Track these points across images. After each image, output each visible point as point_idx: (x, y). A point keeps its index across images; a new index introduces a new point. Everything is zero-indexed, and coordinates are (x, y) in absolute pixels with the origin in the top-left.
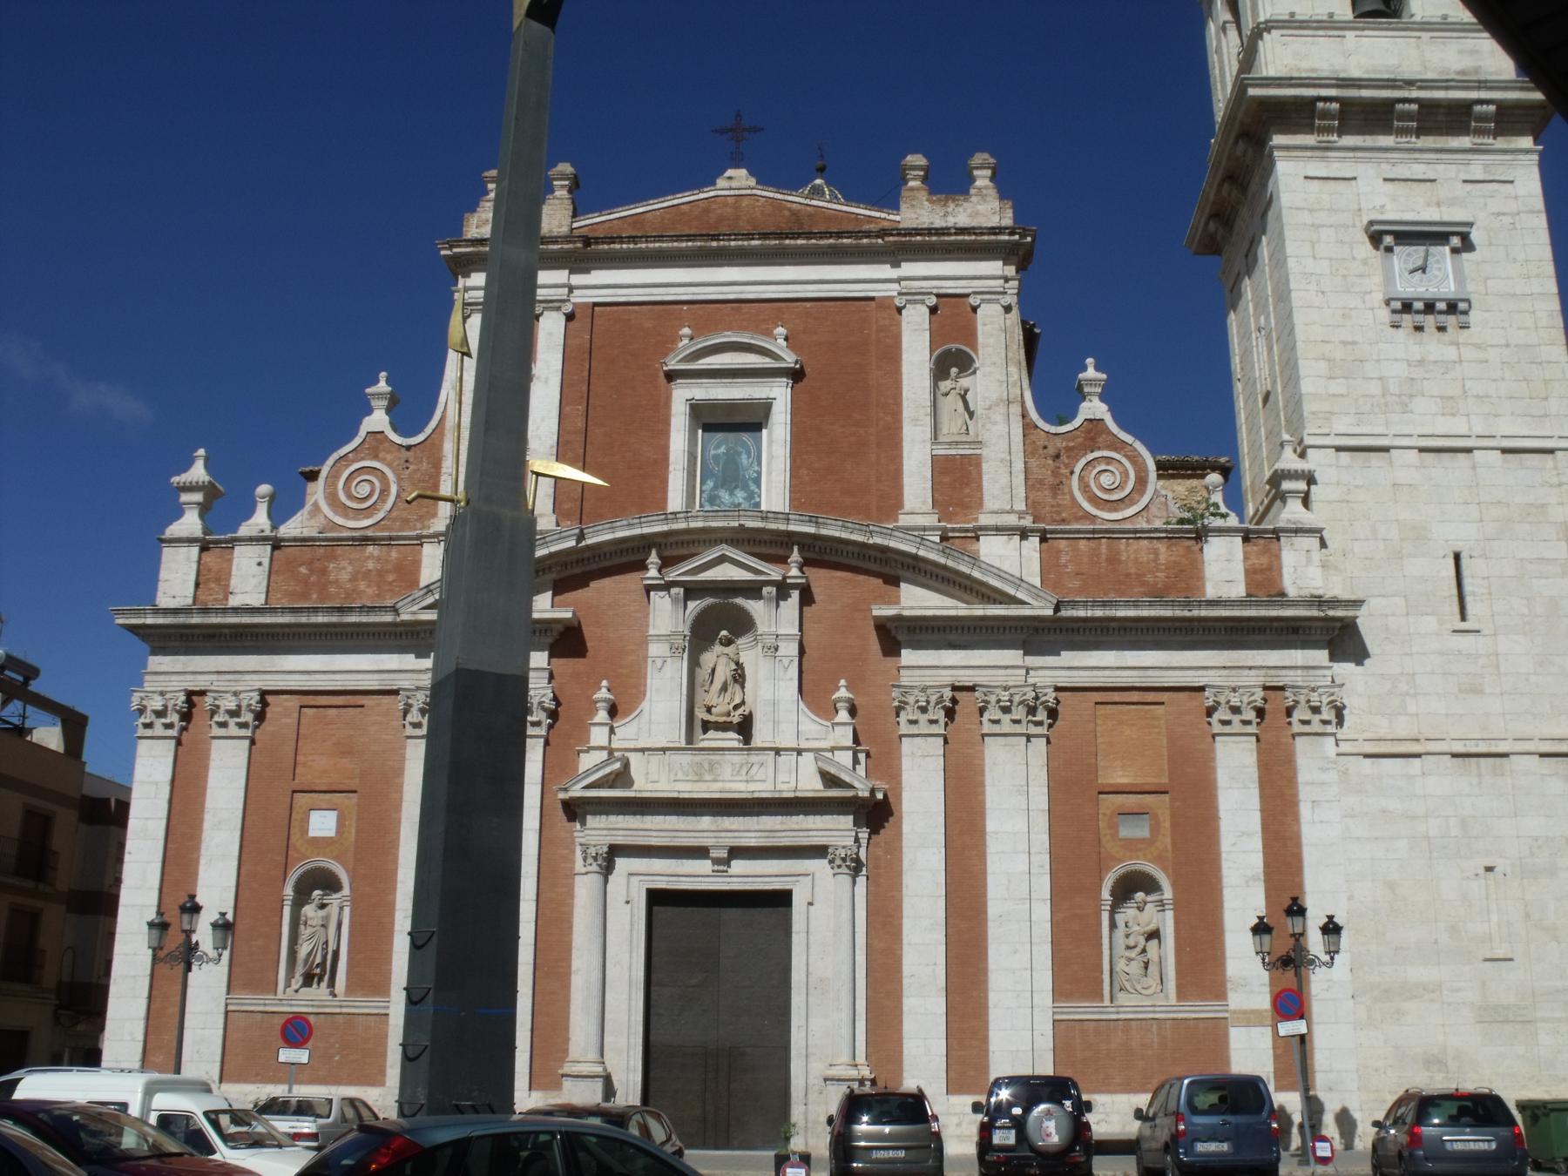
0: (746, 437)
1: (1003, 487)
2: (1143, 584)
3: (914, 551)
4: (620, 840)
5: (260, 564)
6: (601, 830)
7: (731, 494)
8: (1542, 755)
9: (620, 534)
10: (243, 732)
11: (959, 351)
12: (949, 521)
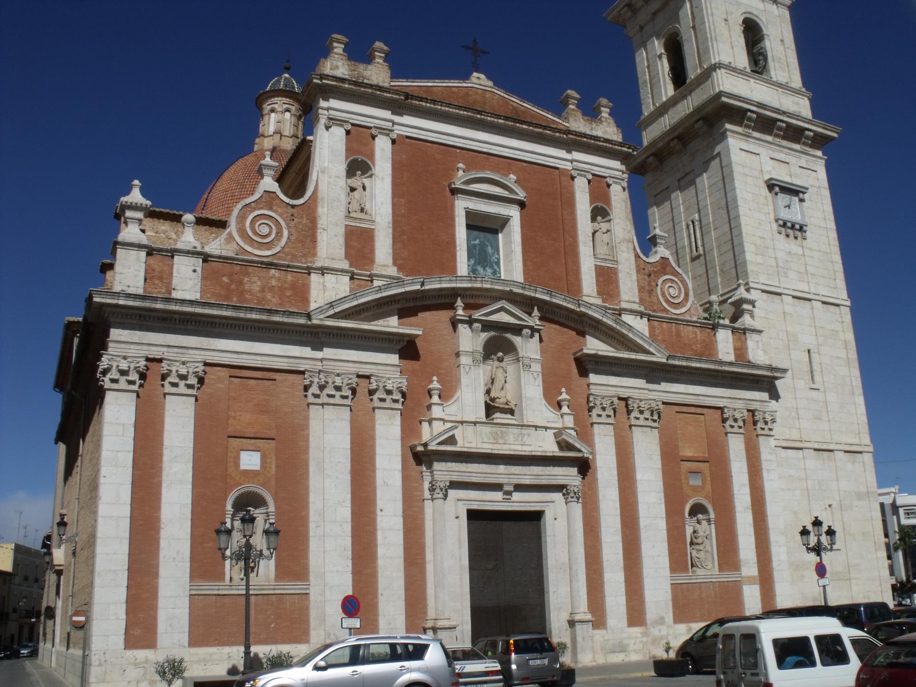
0: (489, 236)
1: (629, 288)
2: (692, 350)
4: (455, 478)
5: (195, 271)
6: (444, 471)
7: (484, 269)
8: (846, 452)
9: (444, 285)
10: (190, 392)
11: (602, 207)
12: (357, 268)
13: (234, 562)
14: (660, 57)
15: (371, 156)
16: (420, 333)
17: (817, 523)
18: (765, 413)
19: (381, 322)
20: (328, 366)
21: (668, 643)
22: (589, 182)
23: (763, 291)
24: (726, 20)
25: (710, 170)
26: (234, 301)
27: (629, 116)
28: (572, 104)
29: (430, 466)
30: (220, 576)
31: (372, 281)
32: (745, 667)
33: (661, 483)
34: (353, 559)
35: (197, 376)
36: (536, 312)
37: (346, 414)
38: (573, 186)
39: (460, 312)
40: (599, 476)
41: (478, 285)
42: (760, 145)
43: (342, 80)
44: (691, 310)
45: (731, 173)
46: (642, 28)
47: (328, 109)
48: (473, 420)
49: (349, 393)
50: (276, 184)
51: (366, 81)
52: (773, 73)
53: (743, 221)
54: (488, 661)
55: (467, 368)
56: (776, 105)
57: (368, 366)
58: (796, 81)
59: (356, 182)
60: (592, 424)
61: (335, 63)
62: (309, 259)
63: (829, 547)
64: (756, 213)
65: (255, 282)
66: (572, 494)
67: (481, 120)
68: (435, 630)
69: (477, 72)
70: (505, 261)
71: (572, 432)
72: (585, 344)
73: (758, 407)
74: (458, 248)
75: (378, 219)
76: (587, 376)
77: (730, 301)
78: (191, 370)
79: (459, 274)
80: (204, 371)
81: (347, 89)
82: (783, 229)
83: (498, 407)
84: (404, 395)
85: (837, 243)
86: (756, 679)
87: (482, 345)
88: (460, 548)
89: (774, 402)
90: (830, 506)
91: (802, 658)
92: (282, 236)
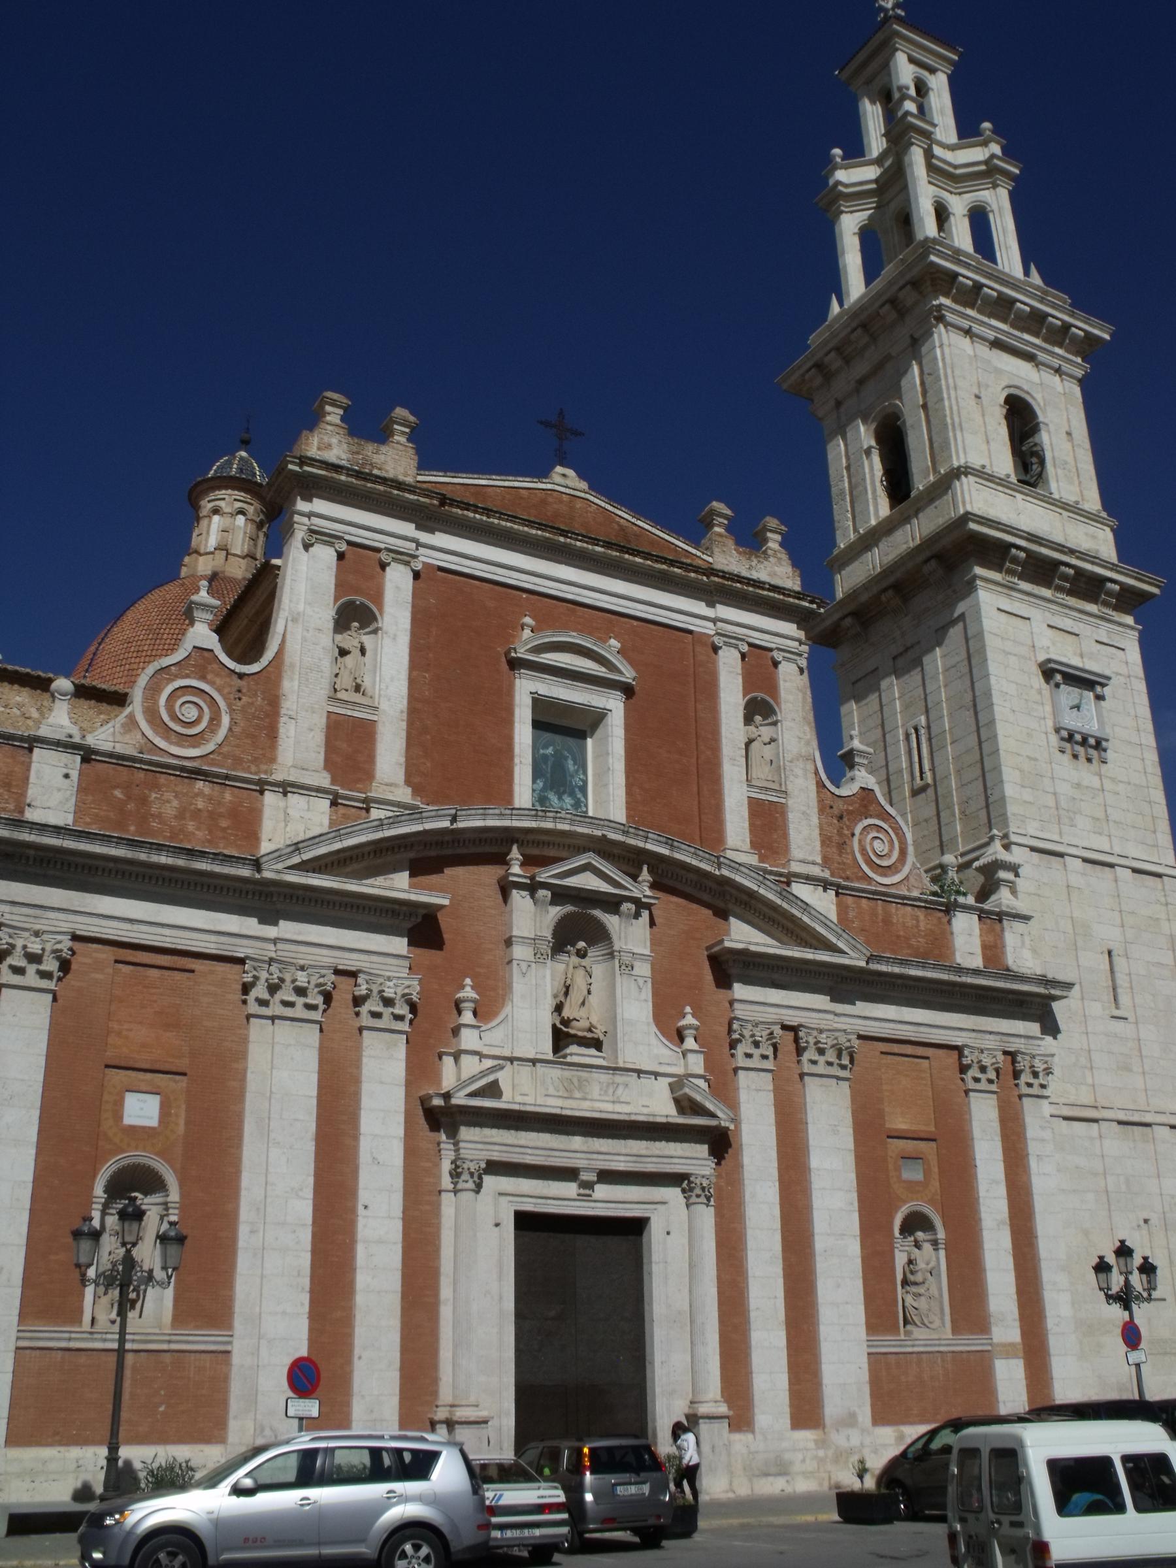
0: (571, 741)
1: (804, 840)
2: (910, 946)
3: (755, 888)
4: (496, 1156)
5: (67, 776)
6: (479, 1144)
7: (560, 798)
13: (102, 1289)
14: (868, 452)
15: (378, 598)
16: (446, 902)
17: (1124, 1251)
18: (1033, 1057)
19: (380, 880)
20: (286, 952)
21: (862, 1462)
22: (743, 656)
23: (1033, 849)
24: (978, 397)
25: (947, 641)
26: (132, 832)
27: (813, 549)
28: (719, 526)
29: (453, 1134)
30: (75, 1316)
31: (368, 810)
32: (1000, 1510)
33: (853, 1176)
34: (312, 1291)
35: (58, 958)
36: (645, 875)
37: (312, 1036)
38: (714, 663)
39: (516, 869)
40: (746, 1160)
41: (549, 825)
42: (1031, 604)
43: (336, 468)
44: (910, 878)
45: (982, 650)
46: (838, 404)
47: (310, 515)
48: (531, 1056)
49: (319, 1000)
50: (215, 637)
51: (375, 472)
52: (1053, 486)
53: (1001, 729)
54: (543, 1484)
55: (524, 965)
56: (1059, 538)
57: (354, 956)
58: (1092, 501)
59: (349, 640)
60: (736, 1070)
61: (326, 439)
62: (263, 767)
63: (1145, 1294)
64: (1023, 717)
65: (168, 801)
66: (698, 1191)
67: (565, 545)
68: (450, 1424)
69: (562, 465)
70: (595, 785)
71: (702, 1083)
72: (728, 933)
73: (1023, 1048)
74: (517, 760)
75: (384, 705)
76: (729, 987)
77: (976, 864)
78: (48, 947)
79: (517, 805)
80: (71, 949)
81: (345, 484)
82: (1068, 745)
83: (575, 1036)
84: (413, 1008)
85: (1158, 771)
86: (1019, 1532)
87: (552, 928)
88: (500, 1279)
89: (1049, 1039)
90: (1146, 1221)
91: (1100, 1497)
92: (219, 725)
